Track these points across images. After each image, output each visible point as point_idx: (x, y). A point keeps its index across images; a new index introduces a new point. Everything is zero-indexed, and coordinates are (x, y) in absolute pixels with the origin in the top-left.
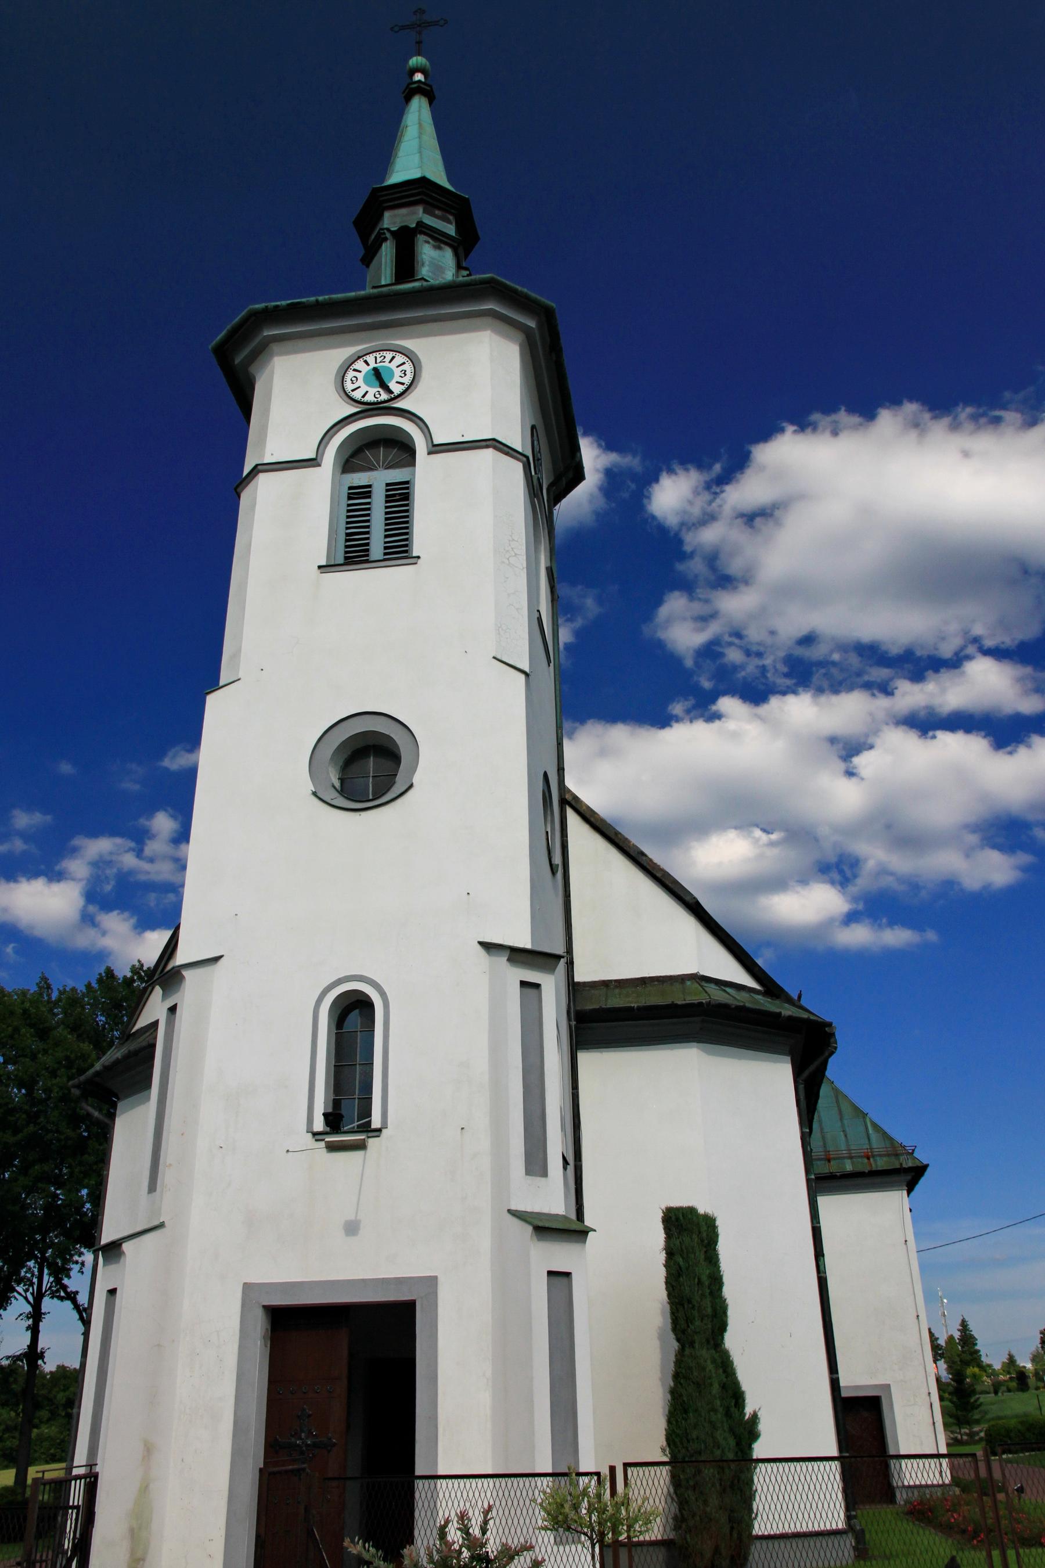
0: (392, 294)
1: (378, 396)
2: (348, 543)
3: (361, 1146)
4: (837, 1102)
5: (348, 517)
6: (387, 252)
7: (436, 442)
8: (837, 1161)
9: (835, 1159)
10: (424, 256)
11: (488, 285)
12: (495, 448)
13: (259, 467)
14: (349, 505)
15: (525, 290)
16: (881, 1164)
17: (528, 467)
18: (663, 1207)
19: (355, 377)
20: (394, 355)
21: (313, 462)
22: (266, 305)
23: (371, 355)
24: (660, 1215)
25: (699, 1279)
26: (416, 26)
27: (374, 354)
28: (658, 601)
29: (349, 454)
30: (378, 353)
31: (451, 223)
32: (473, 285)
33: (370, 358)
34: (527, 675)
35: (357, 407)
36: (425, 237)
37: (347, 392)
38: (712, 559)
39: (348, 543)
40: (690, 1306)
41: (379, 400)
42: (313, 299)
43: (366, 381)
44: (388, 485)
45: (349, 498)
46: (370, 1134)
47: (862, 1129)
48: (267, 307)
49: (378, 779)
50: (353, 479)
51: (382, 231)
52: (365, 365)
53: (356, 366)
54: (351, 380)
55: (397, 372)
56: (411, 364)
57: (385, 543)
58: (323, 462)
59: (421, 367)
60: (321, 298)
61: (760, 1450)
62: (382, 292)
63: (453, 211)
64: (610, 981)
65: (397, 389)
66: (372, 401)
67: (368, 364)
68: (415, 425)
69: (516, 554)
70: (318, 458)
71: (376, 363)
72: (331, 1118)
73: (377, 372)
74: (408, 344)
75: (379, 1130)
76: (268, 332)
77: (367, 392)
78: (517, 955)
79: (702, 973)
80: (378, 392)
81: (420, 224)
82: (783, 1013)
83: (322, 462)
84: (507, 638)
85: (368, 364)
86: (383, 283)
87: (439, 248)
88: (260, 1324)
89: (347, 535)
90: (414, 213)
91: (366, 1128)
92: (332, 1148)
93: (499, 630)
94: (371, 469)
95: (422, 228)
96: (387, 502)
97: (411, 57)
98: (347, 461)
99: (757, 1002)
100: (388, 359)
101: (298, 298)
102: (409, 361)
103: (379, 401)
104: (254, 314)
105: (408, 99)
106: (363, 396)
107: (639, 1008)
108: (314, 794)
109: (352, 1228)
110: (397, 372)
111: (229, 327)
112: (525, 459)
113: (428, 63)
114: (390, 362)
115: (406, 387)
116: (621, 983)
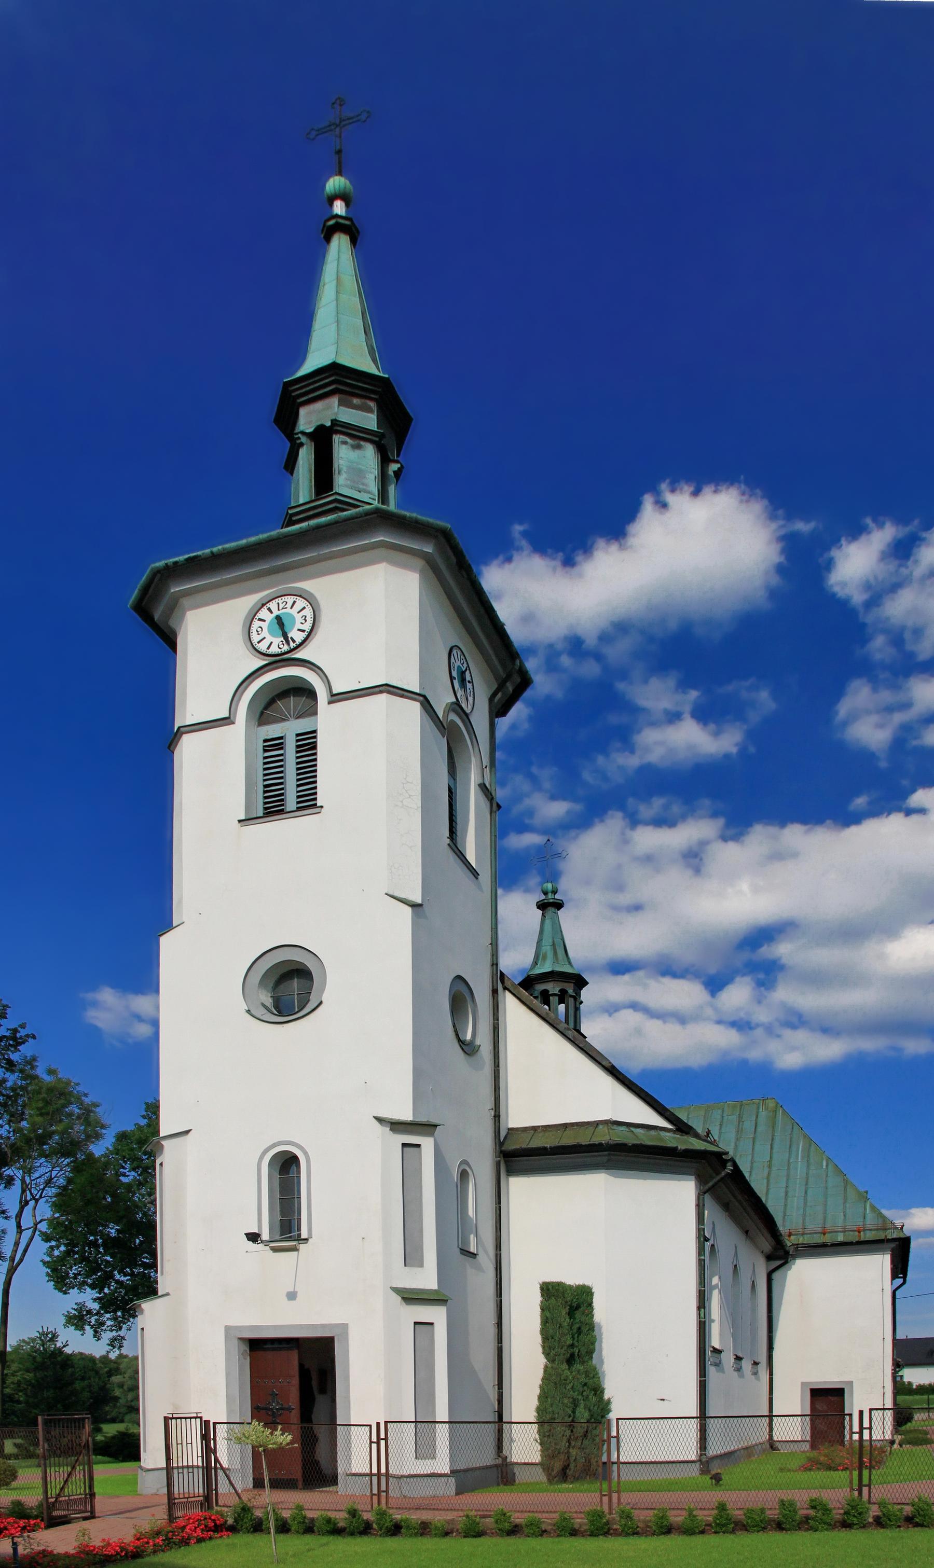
0: (340, 520)
1: (281, 646)
3: (294, 1249)
7: (335, 692)
9: (829, 1232)
10: (341, 462)
11: (376, 515)
12: (389, 692)
13: (181, 729)
14: (265, 758)
16: (869, 1236)
17: (427, 704)
18: (541, 1283)
19: (260, 627)
20: (295, 600)
21: (226, 721)
22: (166, 562)
24: (587, 1283)
27: (277, 600)
28: (838, 692)
29: (263, 706)
30: (280, 599)
31: (371, 411)
33: (273, 605)
34: (414, 906)
35: (267, 660)
38: (897, 639)
41: (283, 650)
42: (207, 551)
44: (298, 735)
45: (265, 751)
46: (300, 1242)
49: (302, 995)
50: (268, 732)
51: (297, 436)
52: (269, 613)
53: (260, 615)
54: (257, 631)
55: (298, 618)
56: (311, 608)
57: (298, 792)
59: (319, 610)
60: (215, 549)
62: (270, 536)
65: (299, 637)
66: (277, 653)
67: (271, 612)
69: (410, 796)
71: (279, 610)
73: (279, 619)
74: (306, 585)
75: (307, 1240)
76: (175, 589)
77: (272, 643)
78: (397, 1126)
79: (614, 1119)
81: (335, 422)
82: (679, 1148)
85: (271, 612)
86: (301, 502)
90: (329, 407)
91: (299, 1239)
92: (275, 1250)
95: (337, 427)
96: (297, 752)
98: (262, 713)
99: (661, 1139)
100: (289, 605)
104: (157, 572)
105: (328, 239)
106: (268, 648)
107: (551, 1148)
108: (248, 1011)
110: (298, 618)
111: (139, 586)
112: (421, 698)
113: (348, 183)
114: (291, 608)
116: (546, 1128)
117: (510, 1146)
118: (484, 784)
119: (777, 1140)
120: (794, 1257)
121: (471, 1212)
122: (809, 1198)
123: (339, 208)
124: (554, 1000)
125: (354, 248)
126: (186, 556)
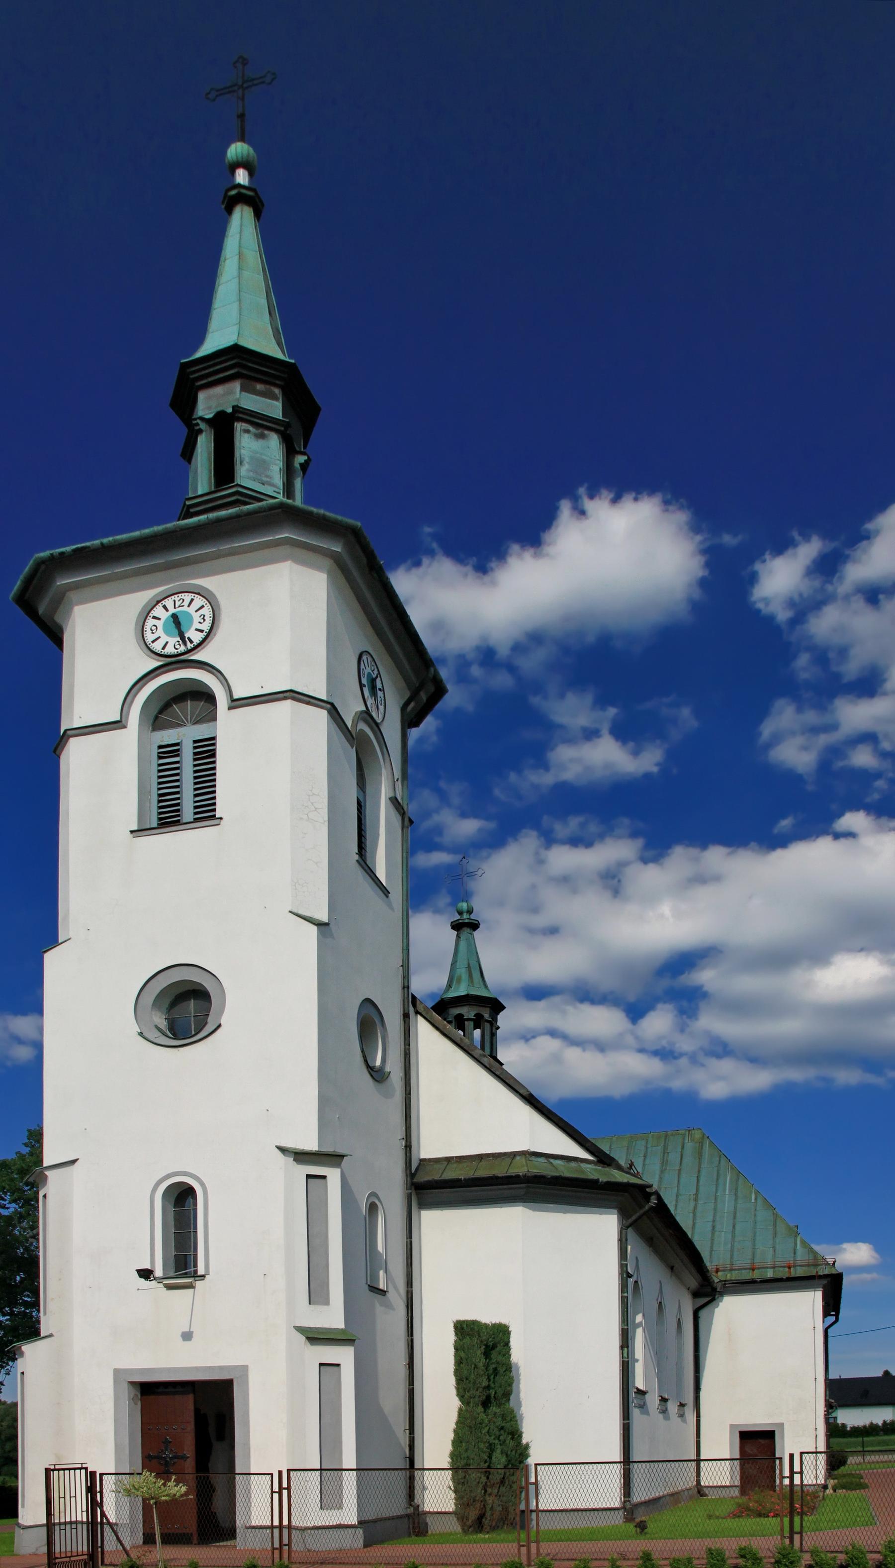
1: (177, 647)
2: (161, 804)
4: (775, 1225)
5: (160, 777)
6: (205, 445)
7: (235, 697)
8: (760, 1270)
9: (759, 1268)
10: (243, 451)
11: (280, 510)
12: (294, 699)
13: (69, 732)
14: (160, 765)
15: (322, 511)
16: (800, 1272)
18: (455, 1321)
19: (154, 625)
21: (118, 725)
22: (51, 552)
23: (169, 598)
24: (504, 1321)
25: (475, 1365)
26: (236, 88)
27: (173, 597)
29: (156, 711)
30: (176, 596)
31: (277, 399)
32: (262, 512)
33: (169, 603)
34: (320, 924)
35: (158, 660)
36: (244, 424)
37: (148, 643)
39: (161, 804)
40: (468, 1381)
42: (97, 542)
43: (166, 631)
44: (195, 742)
45: (160, 758)
46: (196, 1279)
47: (792, 1245)
48: (52, 554)
49: (199, 1018)
50: (163, 737)
53: (155, 613)
54: (151, 629)
55: (196, 617)
56: (210, 607)
58: (129, 723)
60: (105, 541)
61: (531, 1461)
63: (277, 382)
64: (452, 1158)
65: (197, 637)
66: (172, 653)
67: (167, 610)
68: (214, 677)
70: (123, 720)
71: (175, 608)
72: (142, 1273)
75: (203, 1276)
77: (167, 642)
78: (301, 1157)
79: (532, 1150)
80: (178, 641)
81: (236, 409)
82: (601, 1180)
83: (127, 724)
84: (304, 892)
85: (167, 610)
86: (200, 493)
87: (262, 436)
88: (126, 1392)
89: (160, 795)
91: (195, 1275)
92: (169, 1287)
93: (295, 885)
94: (180, 725)
95: (239, 414)
97: (228, 146)
100: (186, 603)
101: (81, 543)
102: (208, 604)
103: (180, 652)
105: (229, 210)
106: (164, 648)
108: (141, 1034)
109: (187, 1336)
110: (196, 617)
111: (22, 577)
112: (329, 706)
113: (251, 151)
115: (206, 634)
116: (461, 1159)
117: (422, 1178)
118: (396, 799)
119: (704, 1173)
120: (722, 1294)
121: (380, 1247)
122: (737, 1232)
123: (242, 177)
124: (469, 1025)
125: (258, 221)
126: (74, 547)
